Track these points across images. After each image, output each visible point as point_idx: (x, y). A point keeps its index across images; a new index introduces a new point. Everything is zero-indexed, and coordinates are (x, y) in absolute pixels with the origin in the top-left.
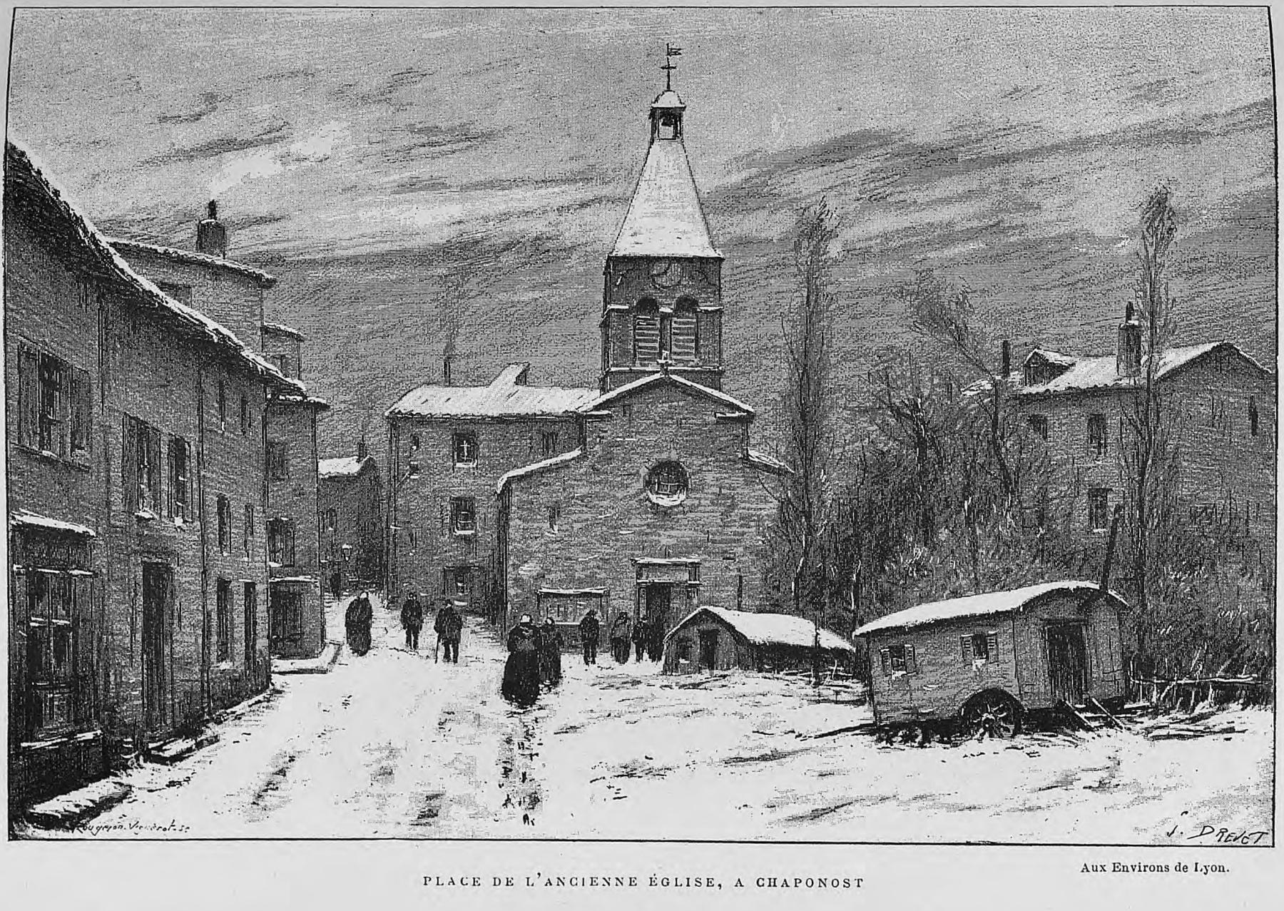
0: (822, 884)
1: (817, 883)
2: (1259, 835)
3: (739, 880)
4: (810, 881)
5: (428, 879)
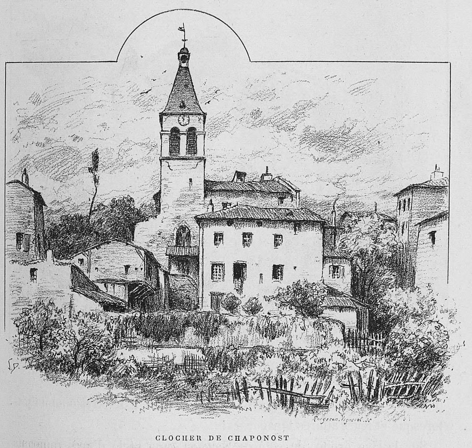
0: (266, 439)
1: (263, 438)
2: (356, 365)
3: (245, 437)
4: (259, 437)
5: (252, 437)
